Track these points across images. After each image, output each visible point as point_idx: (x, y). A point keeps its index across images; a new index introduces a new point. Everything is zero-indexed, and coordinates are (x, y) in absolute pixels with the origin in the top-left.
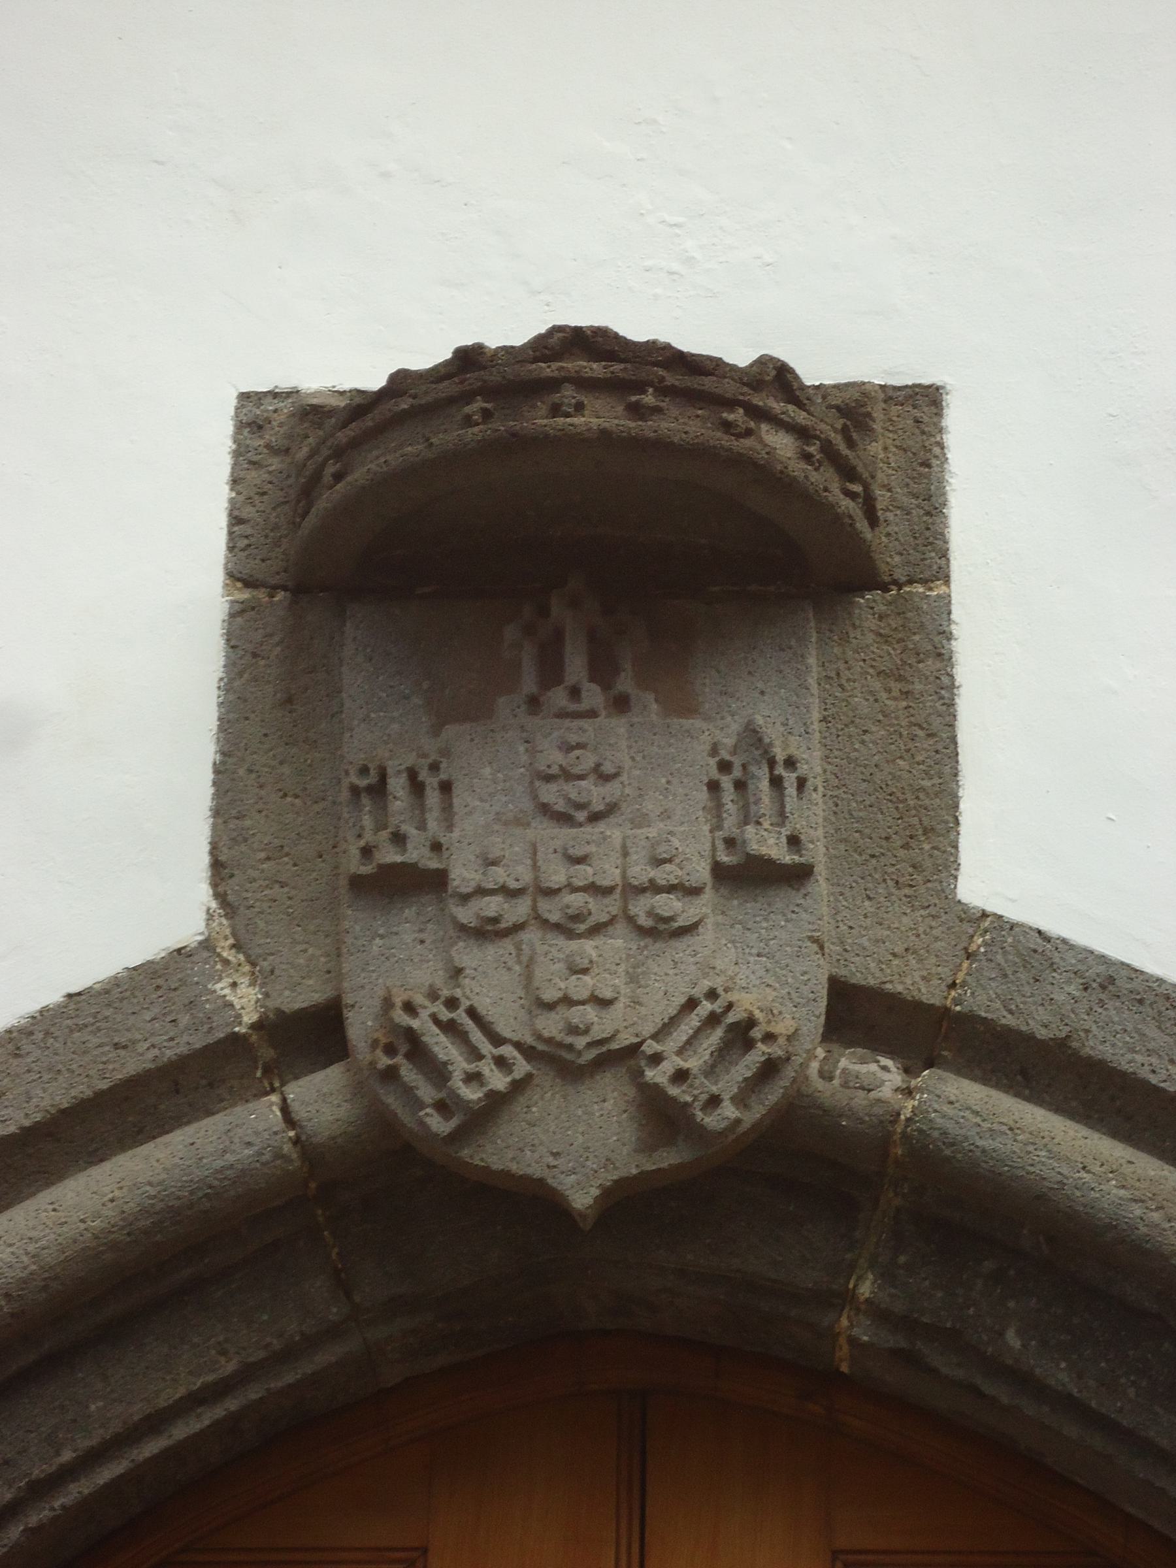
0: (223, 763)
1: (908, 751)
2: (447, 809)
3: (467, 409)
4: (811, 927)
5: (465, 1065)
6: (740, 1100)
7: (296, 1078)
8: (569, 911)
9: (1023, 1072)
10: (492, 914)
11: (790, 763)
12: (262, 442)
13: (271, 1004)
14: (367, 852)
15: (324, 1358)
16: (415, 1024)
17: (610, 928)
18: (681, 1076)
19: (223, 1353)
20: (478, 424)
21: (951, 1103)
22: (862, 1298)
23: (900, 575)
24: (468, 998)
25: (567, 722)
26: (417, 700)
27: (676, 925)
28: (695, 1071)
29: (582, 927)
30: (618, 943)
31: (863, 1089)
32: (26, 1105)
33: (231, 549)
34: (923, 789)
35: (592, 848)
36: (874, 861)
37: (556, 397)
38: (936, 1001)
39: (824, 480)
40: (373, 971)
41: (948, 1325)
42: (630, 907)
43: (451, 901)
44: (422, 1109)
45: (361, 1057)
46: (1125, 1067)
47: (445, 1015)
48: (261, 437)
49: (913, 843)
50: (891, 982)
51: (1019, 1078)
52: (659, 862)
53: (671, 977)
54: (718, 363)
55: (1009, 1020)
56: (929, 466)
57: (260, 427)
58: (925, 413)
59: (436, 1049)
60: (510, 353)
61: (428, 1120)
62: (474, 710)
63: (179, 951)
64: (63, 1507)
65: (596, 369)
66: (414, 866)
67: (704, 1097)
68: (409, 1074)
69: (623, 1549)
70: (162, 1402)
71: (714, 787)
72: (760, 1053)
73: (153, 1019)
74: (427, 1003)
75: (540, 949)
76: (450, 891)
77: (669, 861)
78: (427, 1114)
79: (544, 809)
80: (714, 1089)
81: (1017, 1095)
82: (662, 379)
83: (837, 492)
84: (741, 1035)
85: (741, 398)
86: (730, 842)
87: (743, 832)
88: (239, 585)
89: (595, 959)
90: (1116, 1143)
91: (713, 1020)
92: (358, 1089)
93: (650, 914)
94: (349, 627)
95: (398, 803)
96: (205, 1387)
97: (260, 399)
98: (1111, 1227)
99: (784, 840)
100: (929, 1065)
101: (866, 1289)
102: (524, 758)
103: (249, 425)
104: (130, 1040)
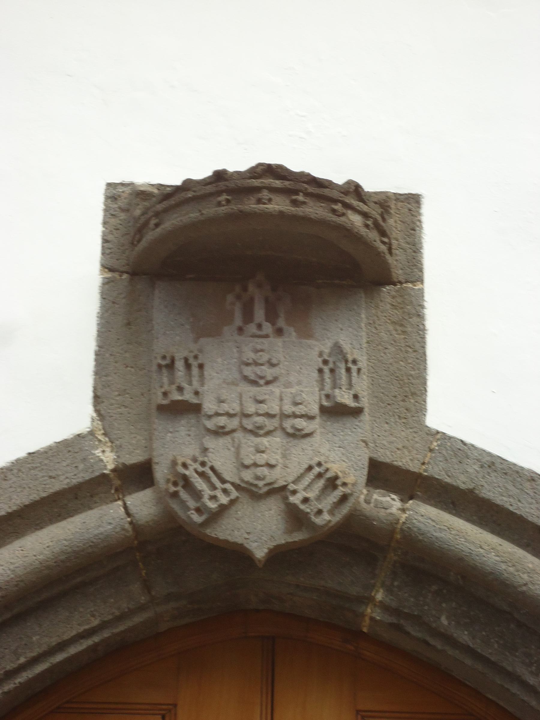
0: (99, 351)
1: (404, 358)
2: (202, 376)
3: (220, 199)
4: (362, 435)
5: (210, 492)
6: (331, 512)
7: (130, 494)
8: (257, 425)
9: (453, 503)
10: (222, 425)
11: (354, 362)
12: (116, 206)
13: (122, 460)
14: (165, 394)
15: (137, 619)
16: (187, 473)
17: (274, 433)
18: (306, 500)
19: (93, 616)
20: (224, 206)
21: (422, 516)
22: (377, 600)
23: (401, 278)
24: (211, 462)
25: (256, 340)
26: (188, 327)
27: (303, 432)
28: (312, 499)
29: (262, 432)
30: (277, 440)
31: (384, 508)
32: (9, 502)
33: (103, 254)
34: (411, 375)
35: (267, 397)
36: (389, 407)
37: (260, 195)
38: (416, 470)
39: (373, 235)
40: (167, 448)
41: (416, 613)
42: (284, 424)
43: (203, 418)
44: (189, 511)
45: (161, 486)
46: (499, 502)
47: (200, 469)
48: (116, 203)
49: (407, 399)
50: (396, 461)
51: (451, 505)
52: (296, 404)
53: (301, 455)
54: (330, 182)
55: (448, 480)
56: (414, 230)
57: (116, 199)
58: (413, 206)
59: (196, 484)
60: (239, 174)
61: (192, 516)
62: (212, 331)
63: (79, 435)
64: (20, 683)
65: (278, 183)
66: (187, 401)
67: (316, 510)
68: (184, 495)
69: (264, 708)
70: (66, 637)
71: (320, 371)
72: (341, 491)
73: (68, 465)
74: (192, 464)
75: (244, 441)
76: (203, 413)
77: (300, 404)
78: (192, 513)
79: (246, 378)
80: (320, 507)
81: (450, 513)
82: (306, 189)
83: (379, 242)
84: (332, 483)
85: (340, 199)
86: (328, 396)
87: (334, 392)
88: (106, 270)
89: (268, 446)
90: (494, 536)
91: (320, 476)
92: (159, 500)
93: (293, 427)
94: (157, 292)
95: (180, 373)
96: (85, 630)
97: (116, 186)
98: (491, 573)
99: (351, 396)
100: (411, 498)
101: (380, 596)
102: (236, 355)
103: (110, 198)
104: (56, 475)
